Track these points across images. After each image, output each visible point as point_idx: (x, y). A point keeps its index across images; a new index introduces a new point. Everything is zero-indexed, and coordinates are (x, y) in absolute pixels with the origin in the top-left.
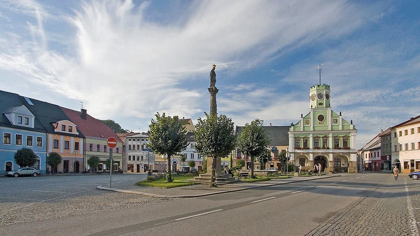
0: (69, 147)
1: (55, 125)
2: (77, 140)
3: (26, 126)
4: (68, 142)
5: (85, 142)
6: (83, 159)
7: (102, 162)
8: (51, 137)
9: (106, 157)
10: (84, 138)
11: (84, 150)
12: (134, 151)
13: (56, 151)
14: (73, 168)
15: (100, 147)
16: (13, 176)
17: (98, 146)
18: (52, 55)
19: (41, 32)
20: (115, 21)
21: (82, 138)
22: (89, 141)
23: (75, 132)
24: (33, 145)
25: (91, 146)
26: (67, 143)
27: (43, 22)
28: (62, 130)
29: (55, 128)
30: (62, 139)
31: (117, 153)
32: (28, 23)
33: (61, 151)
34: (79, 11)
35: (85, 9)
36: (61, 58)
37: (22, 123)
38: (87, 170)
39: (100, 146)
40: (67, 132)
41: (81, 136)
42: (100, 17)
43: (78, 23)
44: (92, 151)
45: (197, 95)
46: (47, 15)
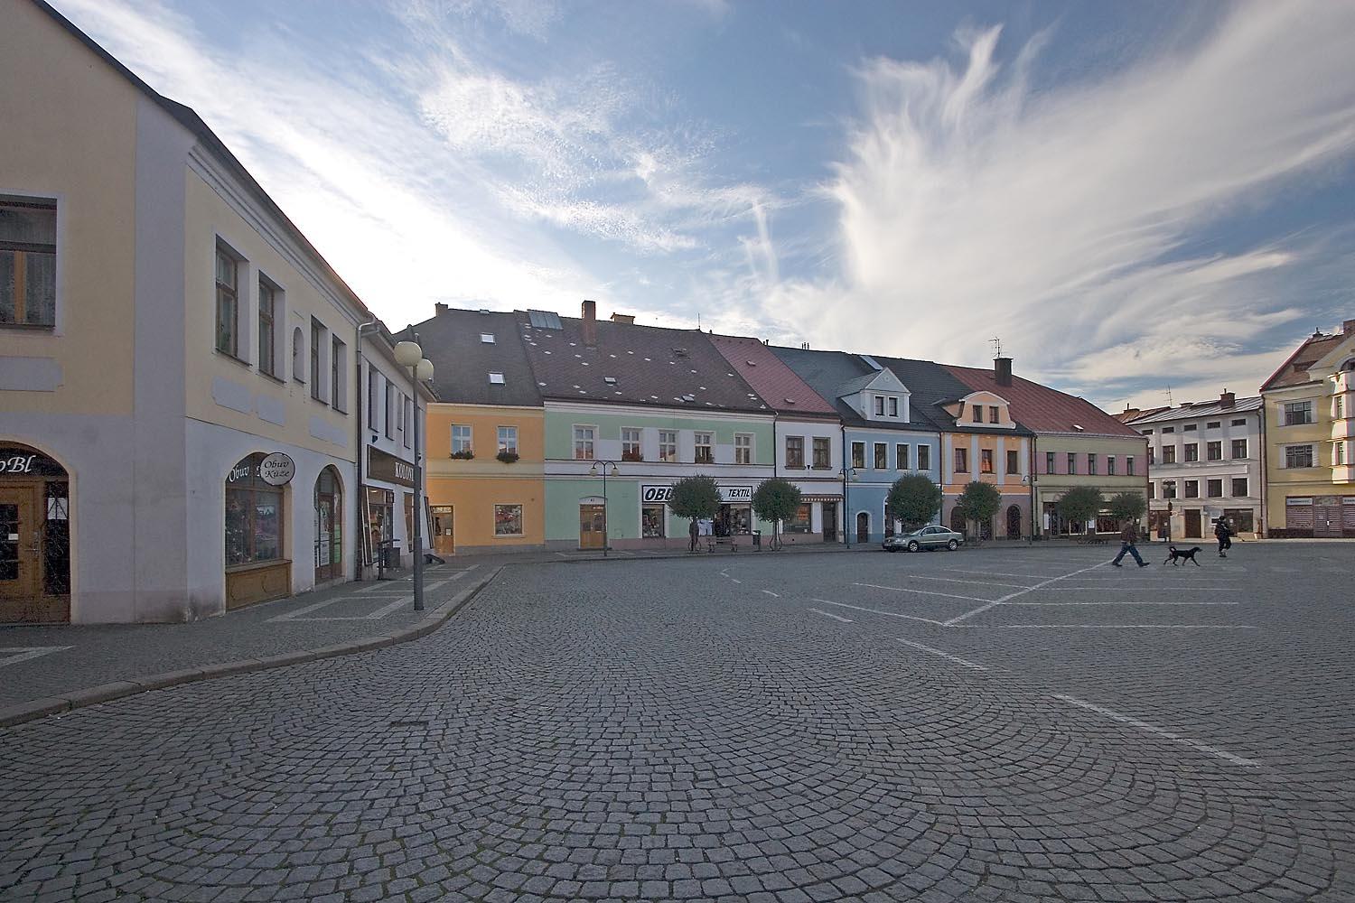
0: (994, 467)
1: (952, 410)
2: (987, 444)
3: (894, 419)
4: (990, 451)
5: (1262, 436)
6: (1029, 502)
7: (808, 496)
8: (948, 439)
9: (1114, 490)
10: (1031, 436)
11: (1033, 474)
12: (1170, 466)
13: (985, 479)
14: (1005, 527)
15: (1057, 458)
16: (908, 550)
17: (1071, 458)
18: (788, 290)
19: (766, 246)
20: (936, 139)
21: (1027, 436)
22: (1044, 445)
23: (1007, 423)
24: (888, 467)
25: (1050, 457)
26: (988, 455)
27: (768, 222)
28: (974, 421)
29: (957, 418)
30: (975, 445)
31: (1090, 474)
32: (740, 238)
33: (1000, 478)
34: (842, 161)
35: (855, 148)
36: (808, 290)
37: (885, 413)
38: (1042, 533)
39: (1057, 455)
40: (986, 423)
41: (1020, 432)
42: (894, 147)
43: (842, 192)
44: (1131, 475)
45: (1277, 260)
46: (776, 204)
